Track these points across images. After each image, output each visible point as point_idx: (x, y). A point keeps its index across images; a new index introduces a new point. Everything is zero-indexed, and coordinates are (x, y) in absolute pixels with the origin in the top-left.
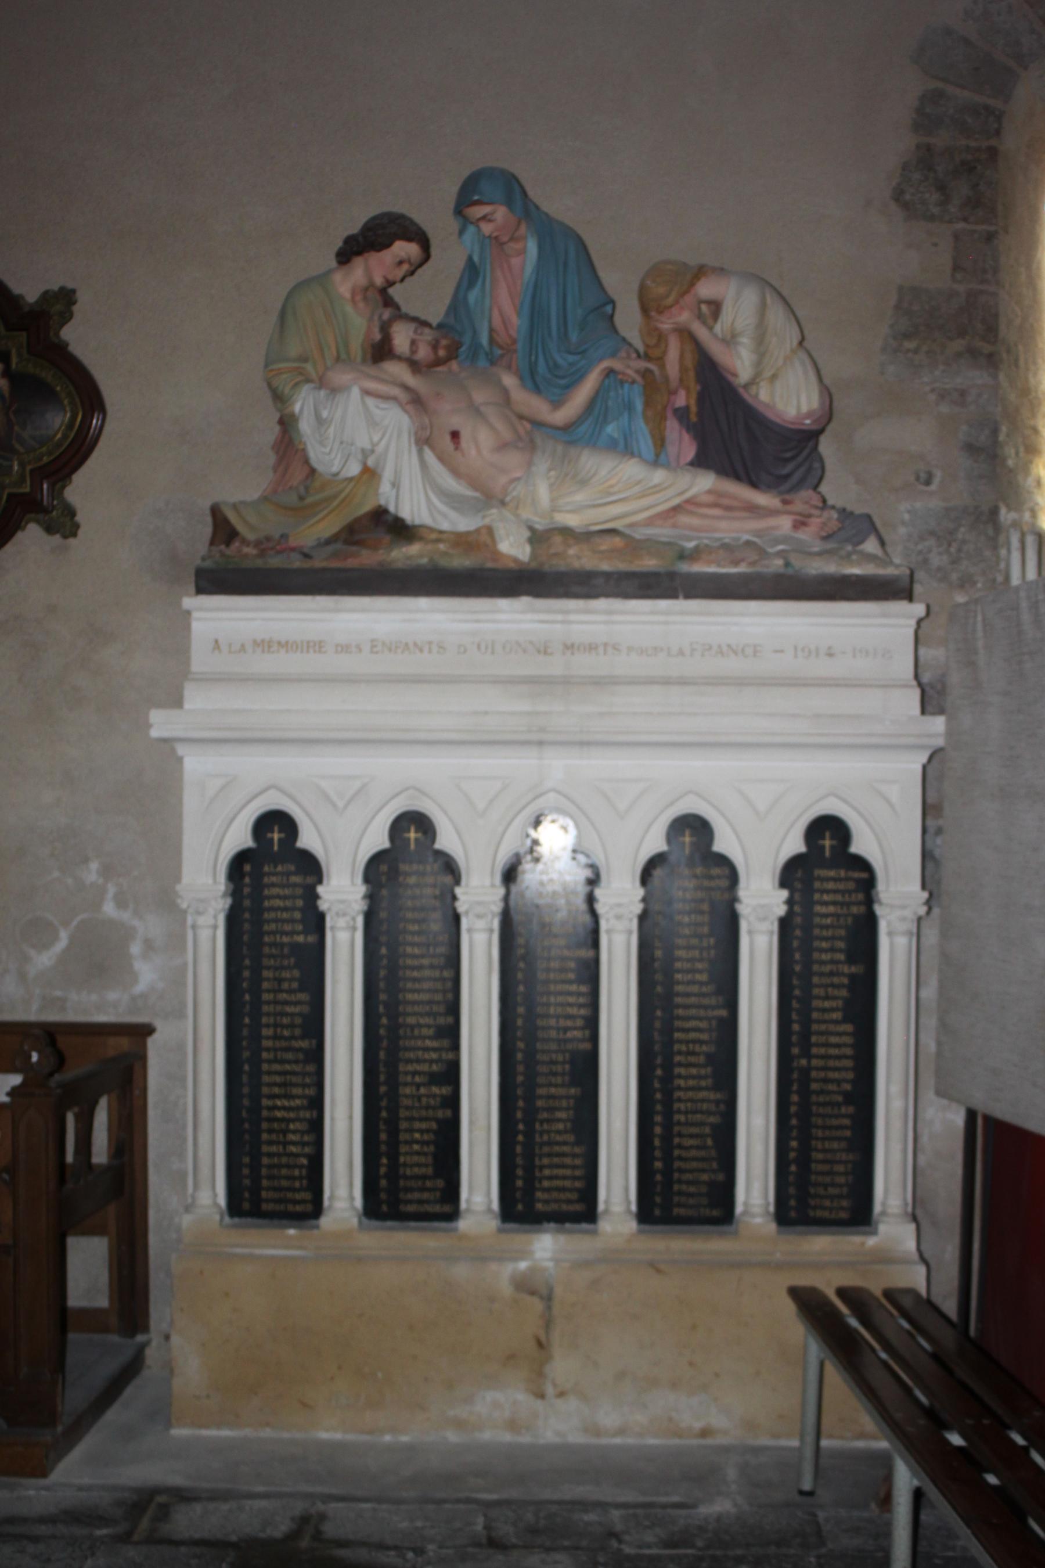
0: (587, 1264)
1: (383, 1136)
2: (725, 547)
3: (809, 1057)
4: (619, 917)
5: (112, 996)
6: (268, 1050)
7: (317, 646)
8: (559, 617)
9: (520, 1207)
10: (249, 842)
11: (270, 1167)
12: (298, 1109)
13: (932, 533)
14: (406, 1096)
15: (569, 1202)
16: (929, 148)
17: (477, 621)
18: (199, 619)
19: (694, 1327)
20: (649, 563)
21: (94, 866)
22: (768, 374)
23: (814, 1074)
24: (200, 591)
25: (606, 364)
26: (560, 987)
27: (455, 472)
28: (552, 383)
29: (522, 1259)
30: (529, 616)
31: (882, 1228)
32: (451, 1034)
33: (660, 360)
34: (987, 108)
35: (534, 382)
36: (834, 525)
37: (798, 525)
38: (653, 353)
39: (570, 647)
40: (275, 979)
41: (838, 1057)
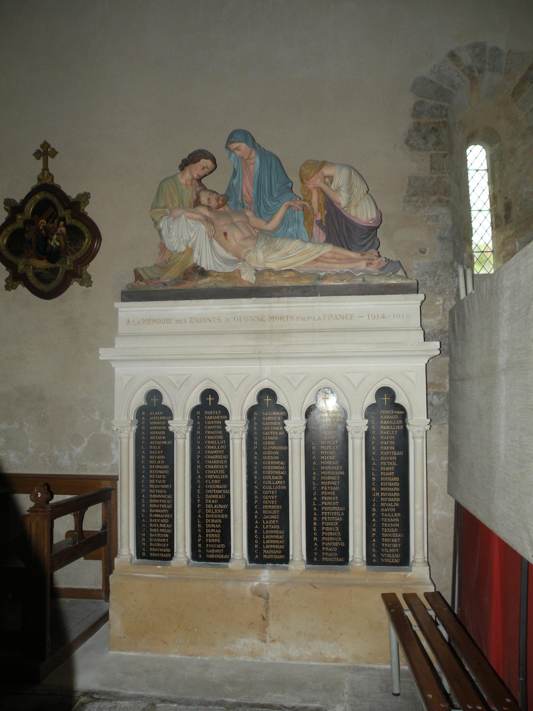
0: (283, 584)
1: (199, 526)
2: (337, 274)
3: (380, 492)
4: (295, 432)
5: (104, 464)
6: (152, 489)
7: (168, 321)
8: (268, 305)
9: (257, 556)
10: (198, 403)
11: (153, 538)
12: (164, 513)
13: (427, 273)
14: (208, 509)
15: (278, 554)
16: (419, 124)
17: (234, 308)
18: (121, 311)
19: (331, 612)
20: (305, 282)
21: (97, 413)
22: (354, 203)
23: (382, 499)
24: (123, 300)
25: (286, 203)
26: (272, 463)
27: (227, 250)
28: (264, 211)
29: (256, 581)
30: (255, 305)
31: (414, 568)
32: (226, 482)
33: (310, 201)
34: (441, 106)
35: (258, 214)
36: (384, 263)
37: (368, 264)
38: (307, 198)
39: (272, 318)
40: (155, 459)
41: (393, 492)
